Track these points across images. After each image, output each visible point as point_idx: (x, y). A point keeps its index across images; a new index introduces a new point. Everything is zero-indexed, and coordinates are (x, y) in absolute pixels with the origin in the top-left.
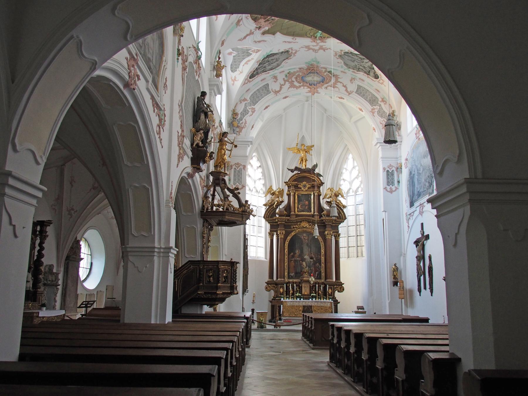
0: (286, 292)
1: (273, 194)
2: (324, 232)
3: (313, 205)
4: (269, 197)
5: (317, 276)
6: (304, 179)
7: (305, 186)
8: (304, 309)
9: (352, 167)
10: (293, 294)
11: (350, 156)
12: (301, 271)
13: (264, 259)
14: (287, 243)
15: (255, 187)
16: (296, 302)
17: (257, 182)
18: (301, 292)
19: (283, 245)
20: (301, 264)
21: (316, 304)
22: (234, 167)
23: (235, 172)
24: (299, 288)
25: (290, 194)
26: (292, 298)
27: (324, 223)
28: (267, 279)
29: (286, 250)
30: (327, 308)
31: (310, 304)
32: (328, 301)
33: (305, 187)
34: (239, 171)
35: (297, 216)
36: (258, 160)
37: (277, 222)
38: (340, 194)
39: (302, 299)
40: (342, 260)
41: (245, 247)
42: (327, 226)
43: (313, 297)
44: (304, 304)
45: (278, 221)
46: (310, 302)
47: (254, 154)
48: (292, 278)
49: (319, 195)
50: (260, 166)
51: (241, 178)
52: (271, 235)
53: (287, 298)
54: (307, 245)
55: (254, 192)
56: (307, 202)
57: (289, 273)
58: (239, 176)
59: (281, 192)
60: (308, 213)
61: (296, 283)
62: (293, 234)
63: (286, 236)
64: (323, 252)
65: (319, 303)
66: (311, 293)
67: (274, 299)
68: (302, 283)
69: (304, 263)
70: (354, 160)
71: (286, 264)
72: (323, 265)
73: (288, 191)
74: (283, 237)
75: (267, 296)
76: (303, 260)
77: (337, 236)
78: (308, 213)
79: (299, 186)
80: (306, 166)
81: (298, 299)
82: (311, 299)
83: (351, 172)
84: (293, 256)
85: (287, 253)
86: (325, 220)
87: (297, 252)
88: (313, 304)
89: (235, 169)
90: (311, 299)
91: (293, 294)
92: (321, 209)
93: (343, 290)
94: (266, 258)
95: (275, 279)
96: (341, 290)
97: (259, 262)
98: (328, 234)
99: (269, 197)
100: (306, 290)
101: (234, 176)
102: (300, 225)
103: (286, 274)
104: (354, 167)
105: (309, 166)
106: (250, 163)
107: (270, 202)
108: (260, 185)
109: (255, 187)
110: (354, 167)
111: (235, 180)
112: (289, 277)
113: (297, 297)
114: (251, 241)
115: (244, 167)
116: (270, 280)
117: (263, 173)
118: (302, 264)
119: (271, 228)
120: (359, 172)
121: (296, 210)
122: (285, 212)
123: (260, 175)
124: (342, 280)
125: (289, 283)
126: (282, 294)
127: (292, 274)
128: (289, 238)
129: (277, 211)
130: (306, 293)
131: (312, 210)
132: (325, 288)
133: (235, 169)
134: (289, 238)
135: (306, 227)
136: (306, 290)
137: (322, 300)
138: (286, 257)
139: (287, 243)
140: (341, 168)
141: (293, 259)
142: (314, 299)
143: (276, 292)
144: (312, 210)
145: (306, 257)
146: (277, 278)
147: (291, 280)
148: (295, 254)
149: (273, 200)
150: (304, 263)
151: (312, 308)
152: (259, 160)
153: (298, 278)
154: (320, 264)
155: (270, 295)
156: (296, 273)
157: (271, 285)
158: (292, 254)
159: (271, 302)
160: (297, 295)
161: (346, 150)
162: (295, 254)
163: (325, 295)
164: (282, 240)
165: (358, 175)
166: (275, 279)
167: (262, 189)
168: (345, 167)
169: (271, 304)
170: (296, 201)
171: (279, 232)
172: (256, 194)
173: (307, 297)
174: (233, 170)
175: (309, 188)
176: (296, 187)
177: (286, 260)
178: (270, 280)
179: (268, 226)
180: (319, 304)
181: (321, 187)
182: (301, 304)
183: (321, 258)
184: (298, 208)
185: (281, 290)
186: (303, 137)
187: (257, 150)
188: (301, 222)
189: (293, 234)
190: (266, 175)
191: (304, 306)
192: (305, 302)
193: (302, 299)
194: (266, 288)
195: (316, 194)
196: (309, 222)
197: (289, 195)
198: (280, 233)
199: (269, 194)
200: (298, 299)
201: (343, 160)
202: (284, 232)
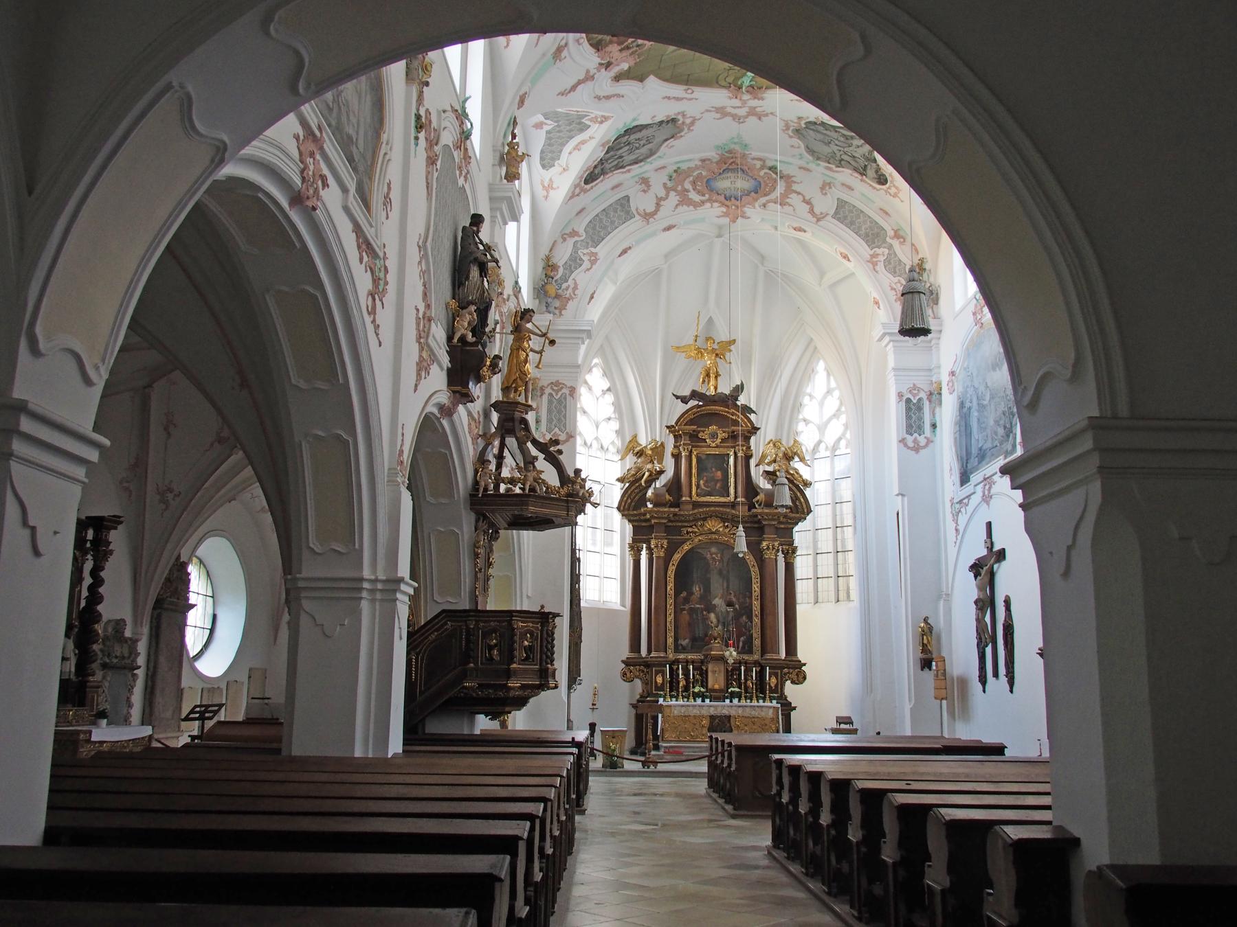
0: (671, 682)
1: (640, 454)
2: (760, 543)
3: (732, 480)
4: (630, 461)
5: (743, 647)
6: (713, 419)
7: (714, 436)
8: (711, 723)
9: (825, 390)
10: (686, 688)
11: (821, 366)
12: (706, 635)
13: (619, 607)
14: (672, 569)
15: (597, 438)
16: (694, 706)
17: (603, 425)
18: (704, 684)
19: (662, 573)
20: (706, 619)
21: (740, 711)
22: (548, 391)
23: (550, 402)
24: (701, 675)
26: (683, 697)
27: (759, 522)
28: (625, 653)
29: (671, 586)
30: (767, 722)
31: (725, 712)
32: (768, 704)
33: (714, 437)
34: (559, 401)
35: (696, 505)
36: (605, 374)
37: (648, 520)
38: (795, 454)
39: (707, 701)
40: (801, 609)
41: (575, 579)
42: (767, 530)
43: (733, 695)
44: (712, 712)
46: (726, 707)
47: (596, 361)
48: (685, 650)
49: (748, 457)
50: (609, 390)
51: (565, 417)
52: (635, 550)
53: (671, 697)
54: (720, 573)
55: (595, 450)
56: (719, 473)
57: (676, 640)
58: (559, 412)
59: (658, 450)
60: (722, 499)
61: (693, 662)
62: (686, 547)
63: (670, 553)
64: (758, 590)
65: (748, 710)
66: (728, 685)
67: (642, 699)
68: (708, 662)
69: (712, 616)
70: (828, 375)
71: (670, 618)
72: (757, 620)
73: (675, 447)
74: (662, 554)
75: (626, 693)
76: (710, 608)
77: (790, 552)
78: (722, 499)
80: (716, 388)
81: (699, 701)
82: (727, 701)
83: (821, 404)
84: (687, 600)
85: (672, 592)
86: (761, 514)
87: (697, 590)
88: (733, 712)
89: (550, 395)
90: (727, 701)
91: (686, 688)
92: (751, 489)
93: (805, 678)
94: (623, 605)
95: (644, 652)
96: (800, 678)
97: (606, 614)
98: (768, 548)
99: (630, 461)
100: (716, 679)
101: (549, 411)
102: (702, 526)
103: (670, 641)
104: (829, 392)
105: (725, 389)
106: (586, 382)
108: (609, 434)
109: (597, 438)
110: (829, 392)
111: (550, 421)
112: (678, 648)
113: (695, 696)
114: (588, 565)
115: (573, 391)
116: (633, 655)
117: (617, 406)
118: (708, 618)
119: (635, 533)
120: (841, 404)
121: (693, 492)
122: (668, 497)
123: (609, 411)
124: (802, 655)
125: (677, 661)
126: (662, 688)
127: (685, 642)
128: (677, 557)
129: (650, 493)
130: (716, 687)
131: (732, 490)
132: (761, 675)
133: (550, 395)
134: (677, 557)
135: (717, 532)
136: (716, 679)
137: (755, 703)
138: (670, 601)
139: (672, 569)
140: (799, 394)
141: (687, 607)
142: (736, 701)
143: (645, 683)
144: (732, 490)
145: (717, 601)
146: (649, 651)
147: (682, 656)
148: (692, 594)
149: (639, 469)
150: (712, 616)
151: (732, 720)
152: (606, 374)
153: (698, 650)
154: (750, 618)
155: (632, 691)
156: (694, 640)
157: (635, 666)
158: (684, 594)
159: (634, 706)
160: (697, 690)
161: (811, 352)
162: (691, 594)
163: (762, 691)
164: (662, 562)
165: (839, 410)
166: (644, 652)
167: (613, 443)
168: (808, 390)
169: (634, 711)
170: (694, 471)
172: (599, 454)
173: (718, 696)
174: (545, 398)
175: (723, 440)
176: (694, 438)
177: (671, 609)
178: (633, 655)
179: (629, 528)
180: (748, 712)
181: (753, 439)
182: (705, 712)
183: (751, 604)
184: (698, 486)
185: (659, 680)
186: (710, 320)
187: (601, 352)
188: (705, 519)
189: (686, 547)
190: (623, 410)
191: (712, 717)
192: (715, 707)
193: (707, 701)
194: (624, 674)
195: (740, 454)
196: (724, 520)
197: (677, 457)
198: (657, 546)
199: (630, 455)
200: (699, 701)
201: (803, 375)
202: (665, 542)
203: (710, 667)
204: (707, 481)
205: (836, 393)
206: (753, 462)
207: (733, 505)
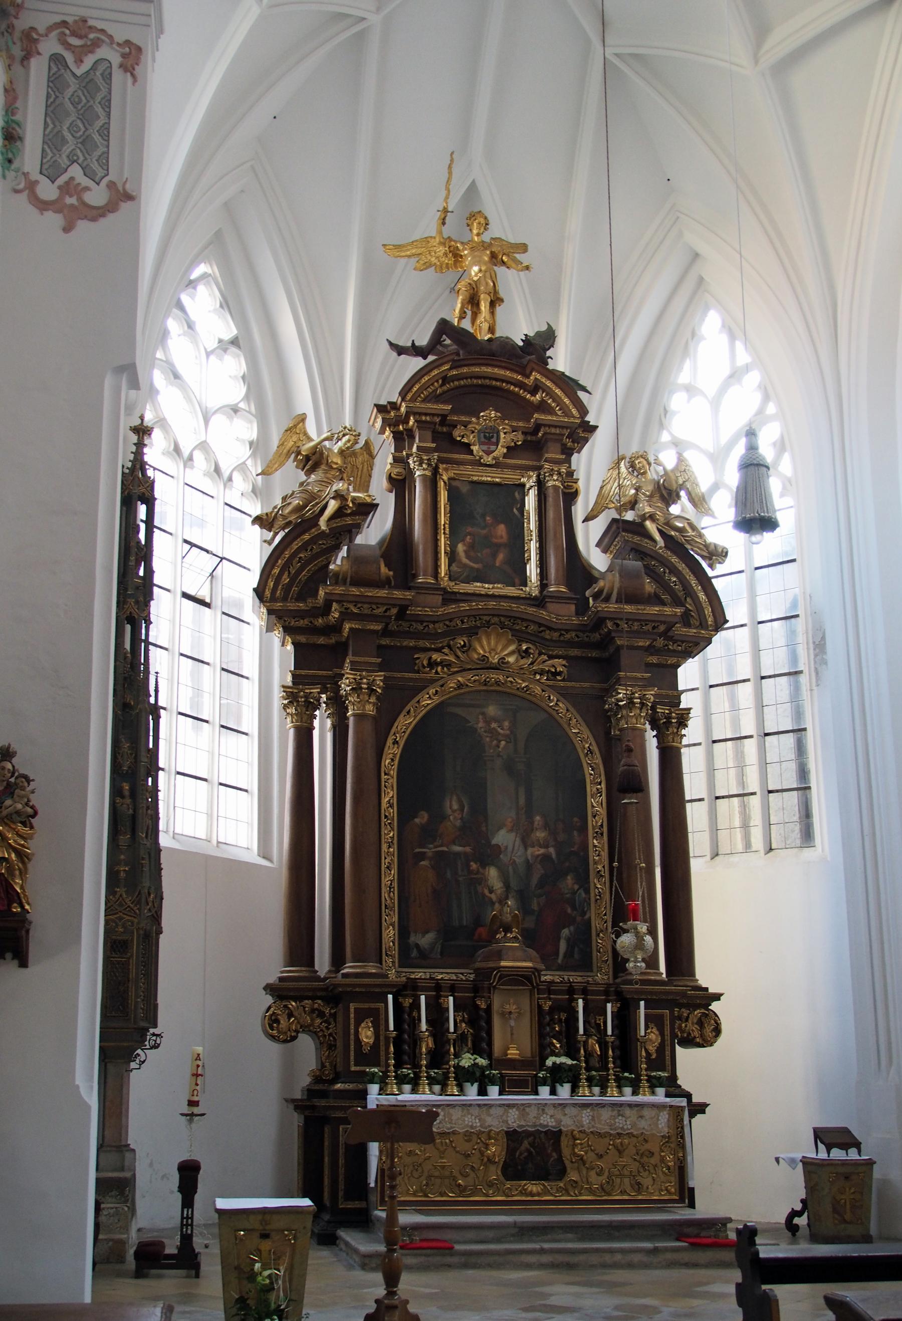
0: (398, 1042)
1: (313, 461)
2: (610, 690)
3: (533, 546)
4: (290, 479)
5: (569, 954)
6: (487, 396)
7: (489, 437)
8: (511, 1151)
9: (727, 372)
10: (437, 1058)
11: (711, 324)
12: (478, 922)
13: (252, 856)
14: (392, 753)
15: (203, 446)
16: (466, 1106)
17: (218, 420)
18: (483, 1045)
19: (370, 754)
20: (476, 881)
21: (586, 1117)
22: (49, 46)
23: (55, 83)
24: (471, 1023)
25: (411, 473)
26: (432, 1081)
27: (607, 641)
28: (273, 965)
29: (389, 795)
30: (654, 1146)
31: (548, 1121)
32: (644, 1098)
33: (491, 440)
34: (87, 82)
35: (450, 597)
36: (225, 304)
37: (336, 628)
38: (682, 487)
39: (494, 1091)
40: (698, 867)
41: (135, 595)
42: (625, 658)
43: (556, 1076)
44: (514, 1120)
45: (346, 615)
46: (549, 1105)
47: (201, 269)
48: (424, 958)
49: (571, 496)
50: (235, 342)
51: (105, 132)
52: (299, 702)
53: (401, 1080)
54: (509, 768)
55: (198, 474)
56: (501, 530)
57: (404, 933)
58: (87, 116)
59: (357, 460)
60: (511, 591)
61: (453, 989)
62: (427, 701)
63: (381, 725)
64: (602, 811)
65: (606, 1114)
66: (543, 1050)
67: (320, 1088)
68: (491, 989)
69: (492, 873)
70: (732, 338)
71: (390, 877)
72: (600, 885)
73: (396, 460)
74: (370, 709)
75: (263, 1078)
76: (488, 854)
77: (670, 721)
78: (511, 591)
79: (457, 434)
80: (492, 330)
81: (472, 1092)
82: (544, 1091)
83: (716, 403)
84: (429, 834)
85: (393, 812)
86: (615, 619)
87: (453, 807)
88: (567, 1123)
89: (56, 59)
90: (544, 1091)
91: (437, 1058)
92: (577, 570)
93: (717, 1031)
94: (265, 854)
95: (322, 962)
96: (707, 1032)
97: (217, 868)
98: (631, 703)
99: (290, 479)
100: (513, 1037)
101: (53, 110)
102: (467, 648)
103: (390, 934)
104: (735, 375)
105: (517, 326)
106: (180, 307)
107: (299, 509)
108: (235, 441)
109: (203, 446)
110: (735, 375)
111: (52, 141)
112: (405, 960)
113: (464, 1076)
114: (179, 745)
115: (132, 57)
116: (294, 971)
117: (252, 382)
118: (482, 880)
119: (299, 662)
120: (766, 398)
121: (441, 561)
122: (384, 570)
123: (236, 393)
124: (706, 973)
125: (412, 987)
126: (372, 1056)
127: (425, 940)
128: (405, 723)
129: (339, 561)
130: (513, 1053)
131: (532, 570)
132: (625, 1020)
133: (56, 59)
134: (405, 723)
135: (501, 666)
136: (513, 1037)
137: (613, 1096)
138: (390, 834)
139: (392, 753)
140: (661, 386)
141: (429, 850)
142: (564, 1091)
143: (326, 1044)
144: (532, 570)
145: (503, 838)
146: (338, 960)
147: (419, 974)
148: (443, 817)
149: (311, 497)
150: (492, 873)
151: (564, 1141)
152: (230, 303)
153: (463, 958)
154: (584, 880)
155: (288, 1068)
156: (447, 933)
157: (303, 1000)
158: (422, 818)
159: (298, 1106)
160: (466, 1060)
161: (692, 286)
162: (439, 817)
163: (627, 1061)
164: (368, 726)
165: (760, 411)
166: (322, 962)
167: (242, 467)
168: (684, 377)
169: (297, 1120)
170: (443, 519)
171: (345, 686)
172: (207, 485)
173: (519, 1078)
174: (38, 68)
175: (512, 450)
176: (445, 440)
177: (389, 854)
178: (294, 971)
179: (283, 654)
180: (605, 1120)
181: (575, 456)
182: (494, 1122)
183: (585, 847)
184: (452, 557)
185: (367, 1035)
186: (473, 189)
187: (217, 246)
188: (472, 632)
189: (427, 701)
190: (264, 385)
191: (513, 1136)
192: (522, 1108)
193: (494, 1091)
194: (272, 1021)
195: (553, 482)
196: (520, 637)
197: (400, 485)
198: (357, 689)
199: (291, 464)
200: (472, 1092)
201: (672, 341)
202: (379, 679)
203: (497, 1002)
204: (471, 547)
205: (754, 378)
206: (580, 510)
207: (540, 601)
